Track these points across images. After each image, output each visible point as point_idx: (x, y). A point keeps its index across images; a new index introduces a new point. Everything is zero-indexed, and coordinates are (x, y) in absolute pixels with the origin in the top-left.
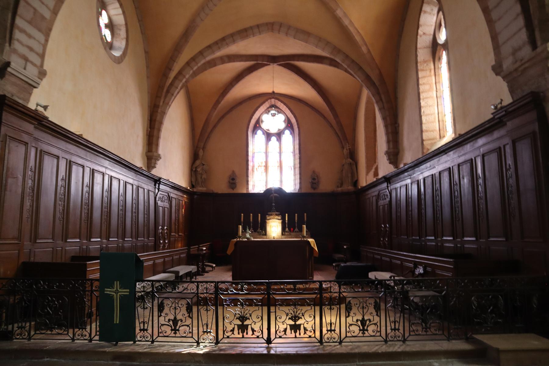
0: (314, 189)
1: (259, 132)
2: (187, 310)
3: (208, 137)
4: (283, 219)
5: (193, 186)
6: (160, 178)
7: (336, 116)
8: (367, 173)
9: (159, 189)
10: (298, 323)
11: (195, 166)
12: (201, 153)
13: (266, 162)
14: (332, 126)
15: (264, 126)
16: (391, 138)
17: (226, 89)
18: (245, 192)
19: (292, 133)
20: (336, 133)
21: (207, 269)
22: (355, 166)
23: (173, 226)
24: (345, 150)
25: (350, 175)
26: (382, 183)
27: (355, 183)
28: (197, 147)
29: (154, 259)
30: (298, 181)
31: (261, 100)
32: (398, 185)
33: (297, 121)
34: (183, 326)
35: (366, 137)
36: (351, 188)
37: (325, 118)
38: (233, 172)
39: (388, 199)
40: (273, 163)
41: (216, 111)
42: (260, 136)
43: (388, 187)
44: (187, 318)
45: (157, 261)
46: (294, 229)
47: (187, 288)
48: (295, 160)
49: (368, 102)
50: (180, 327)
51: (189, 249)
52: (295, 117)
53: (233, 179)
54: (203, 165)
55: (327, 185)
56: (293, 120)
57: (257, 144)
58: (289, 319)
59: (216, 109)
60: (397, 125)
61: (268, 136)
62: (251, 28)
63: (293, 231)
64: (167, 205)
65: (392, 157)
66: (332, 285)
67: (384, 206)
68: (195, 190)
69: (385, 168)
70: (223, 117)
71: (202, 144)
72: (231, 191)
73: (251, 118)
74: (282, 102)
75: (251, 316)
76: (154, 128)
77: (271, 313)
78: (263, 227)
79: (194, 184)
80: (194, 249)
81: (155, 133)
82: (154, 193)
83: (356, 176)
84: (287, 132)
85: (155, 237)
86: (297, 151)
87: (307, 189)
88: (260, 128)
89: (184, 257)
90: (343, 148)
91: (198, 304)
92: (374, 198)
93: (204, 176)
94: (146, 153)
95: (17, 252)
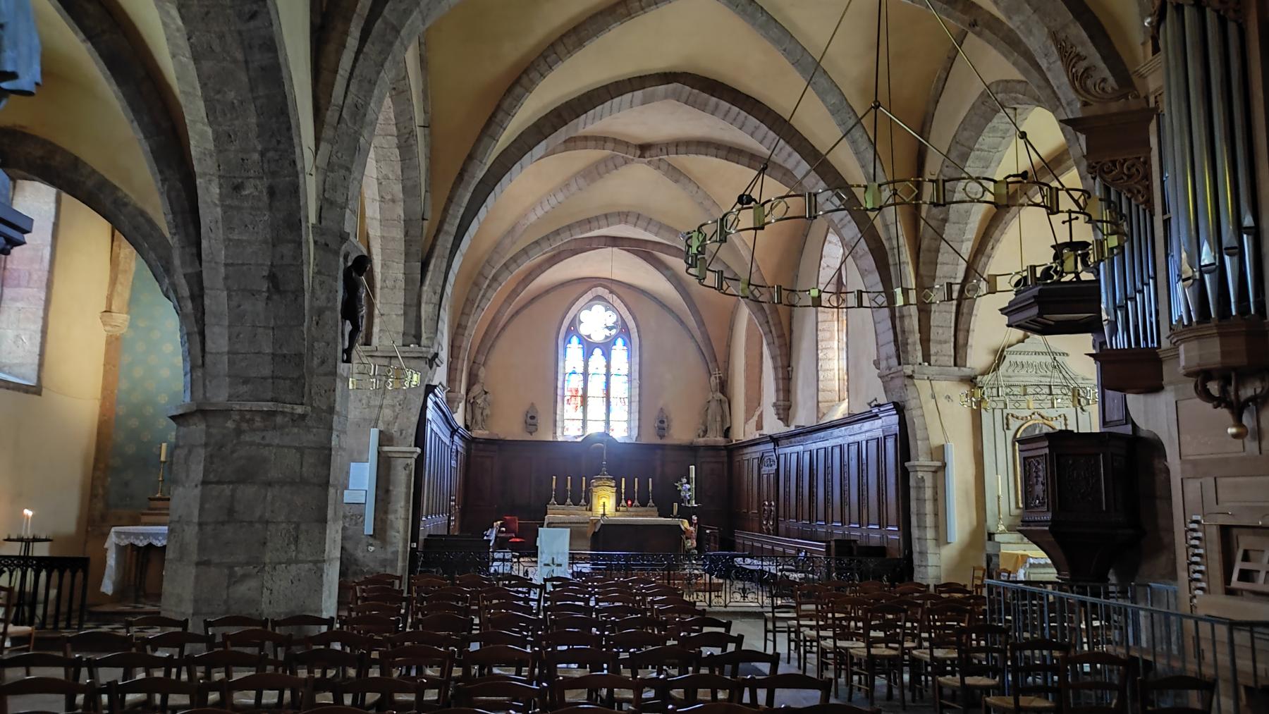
0: (662, 437)
1: (575, 340)
4: (618, 486)
7: (701, 323)
8: (747, 420)
11: (471, 395)
12: (482, 373)
13: (585, 389)
15: (583, 330)
17: (530, 274)
19: (628, 344)
25: (719, 419)
26: (767, 442)
27: (727, 433)
31: (580, 288)
32: (788, 450)
36: (720, 440)
37: (682, 322)
48: (630, 388)
49: (750, 320)
55: (681, 433)
57: (573, 356)
61: (588, 347)
62: (597, 218)
67: (768, 475)
69: (773, 426)
72: (528, 437)
78: (586, 500)
84: (620, 342)
86: (636, 375)
91: (728, 543)
93: (487, 412)
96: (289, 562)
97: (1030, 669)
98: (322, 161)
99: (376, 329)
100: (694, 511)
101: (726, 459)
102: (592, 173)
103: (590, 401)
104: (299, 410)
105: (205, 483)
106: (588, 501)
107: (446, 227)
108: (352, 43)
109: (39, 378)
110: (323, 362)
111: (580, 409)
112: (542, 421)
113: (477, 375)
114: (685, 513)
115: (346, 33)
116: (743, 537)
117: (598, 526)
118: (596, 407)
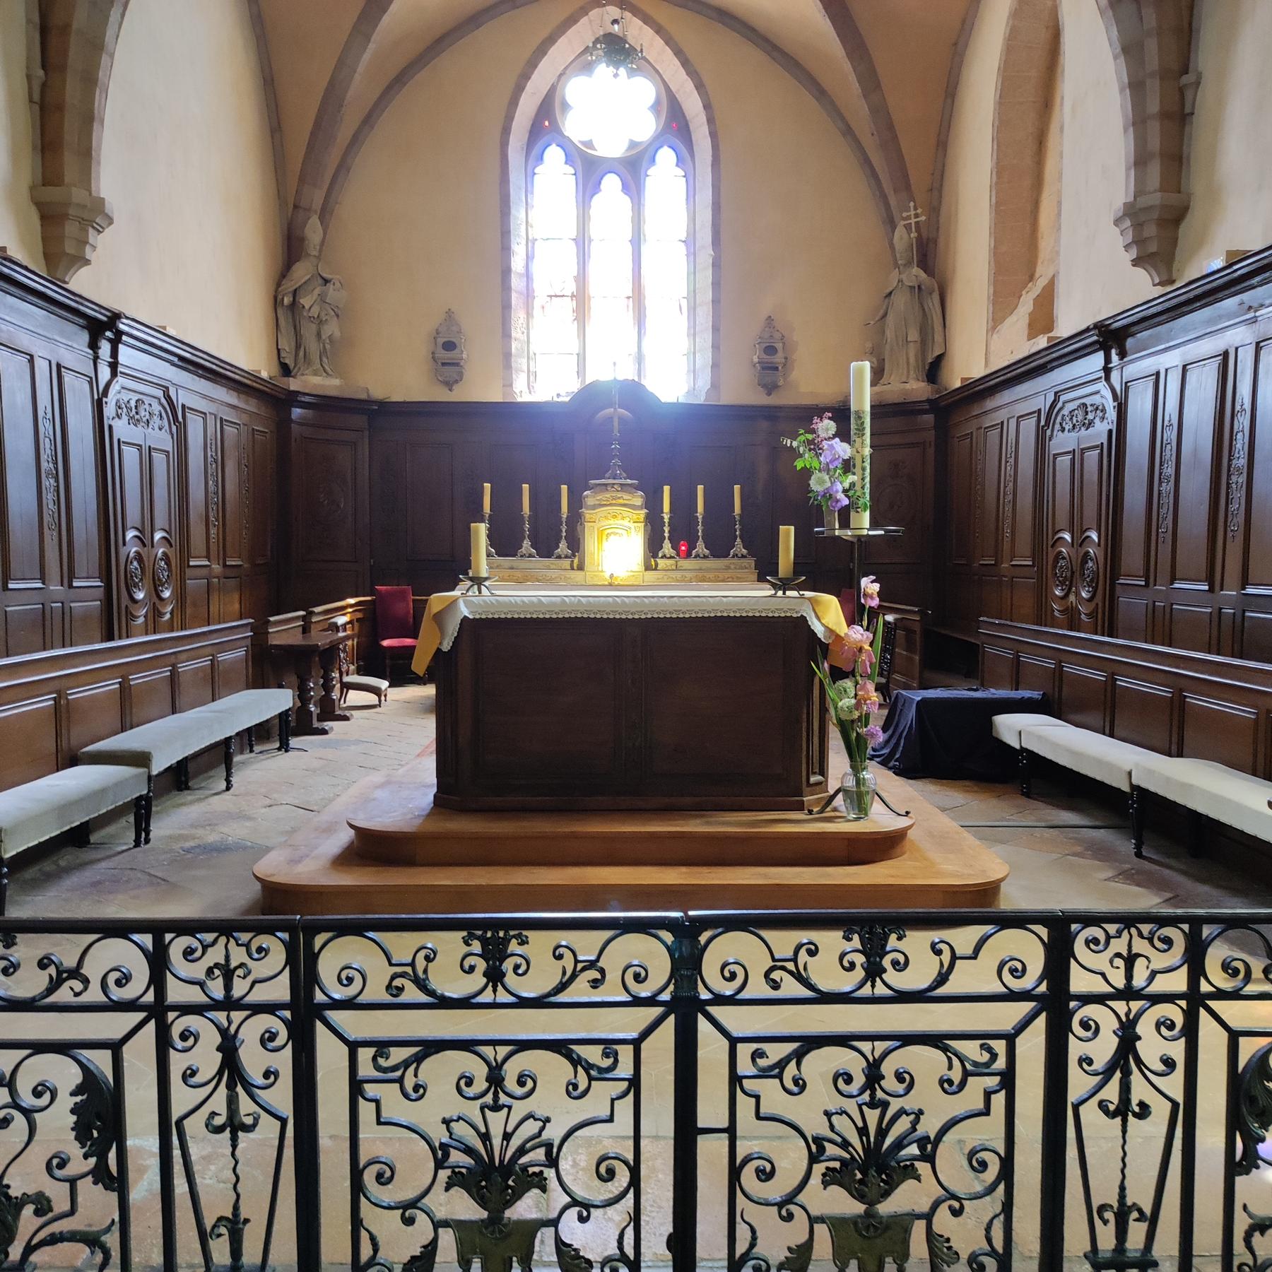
0: (771, 388)
1: (554, 154)
2: (81, 1132)
3: (343, 167)
5: (286, 370)
6: (116, 316)
7: (871, 82)
8: (996, 321)
9: (114, 366)
10: (886, 1208)
11: (289, 285)
12: (313, 232)
13: (581, 279)
14: (848, 131)
15: (574, 126)
16: (1155, 143)
18: (494, 395)
19: (686, 158)
20: (866, 162)
21: (354, 697)
22: (936, 297)
23: (197, 531)
24: (900, 232)
25: (914, 335)
27: (933, 371)
28: (296, 207)
29: (59, 689)
30: (705, 358)
32: (1172, 360)
33: (707, 107)
34: (53, 1240)
35: (1001, 170)
37: (820, 92)
38: (449, 313)
39: (1102, 429)
40: (605, 273)
41: (372, 46)
42: (554, 174)
43: (1107, 370)
44: (85, 1186)
45: (76, 694)
46: (692, 546)
47: (75, 973)
48: (693, 273)
50: (29, 1249)
51: (260, 631)
52: (700, 86)
53: (449, 346)
54: (326, 281)
56: (693, 105)
57: (546, 198)
58: (830, 1178)
59: (368, 39)
60: (1185, 79)
61: (589, 170)
63: (688, 555)
64: (161, 438)
65: (1151, 230)
66: (1140, 946)
67: (1077, 456)
68: (294, 385)
70: (400, 80)
71: (317, 198)
73: (519, 89)
75: (553, 1162)
76: (63, 68)
77: (703, 1143)
78: (557, 536)
79: (289, 361)
80: (285, 630)
81: (72, 90)
82: (93, 381)
83: (938, 337)
84: (666, 156)
85: (106, 574)
86: (705, 236)
87: (742, 391)
88: (556, 130)
89: (235, 661)
90: (891, 223)
92: (1029, 426)
93: (332, 328)
94: (32, 188)
95: (75, 584)
100: (863, 556)
101: (930, 436)
103: (597, 307)
106: (576, 545)
112: (474, 356)
113: (302, 240)
114: (828, 567)
116: (998, 634)
117: (452, 628)
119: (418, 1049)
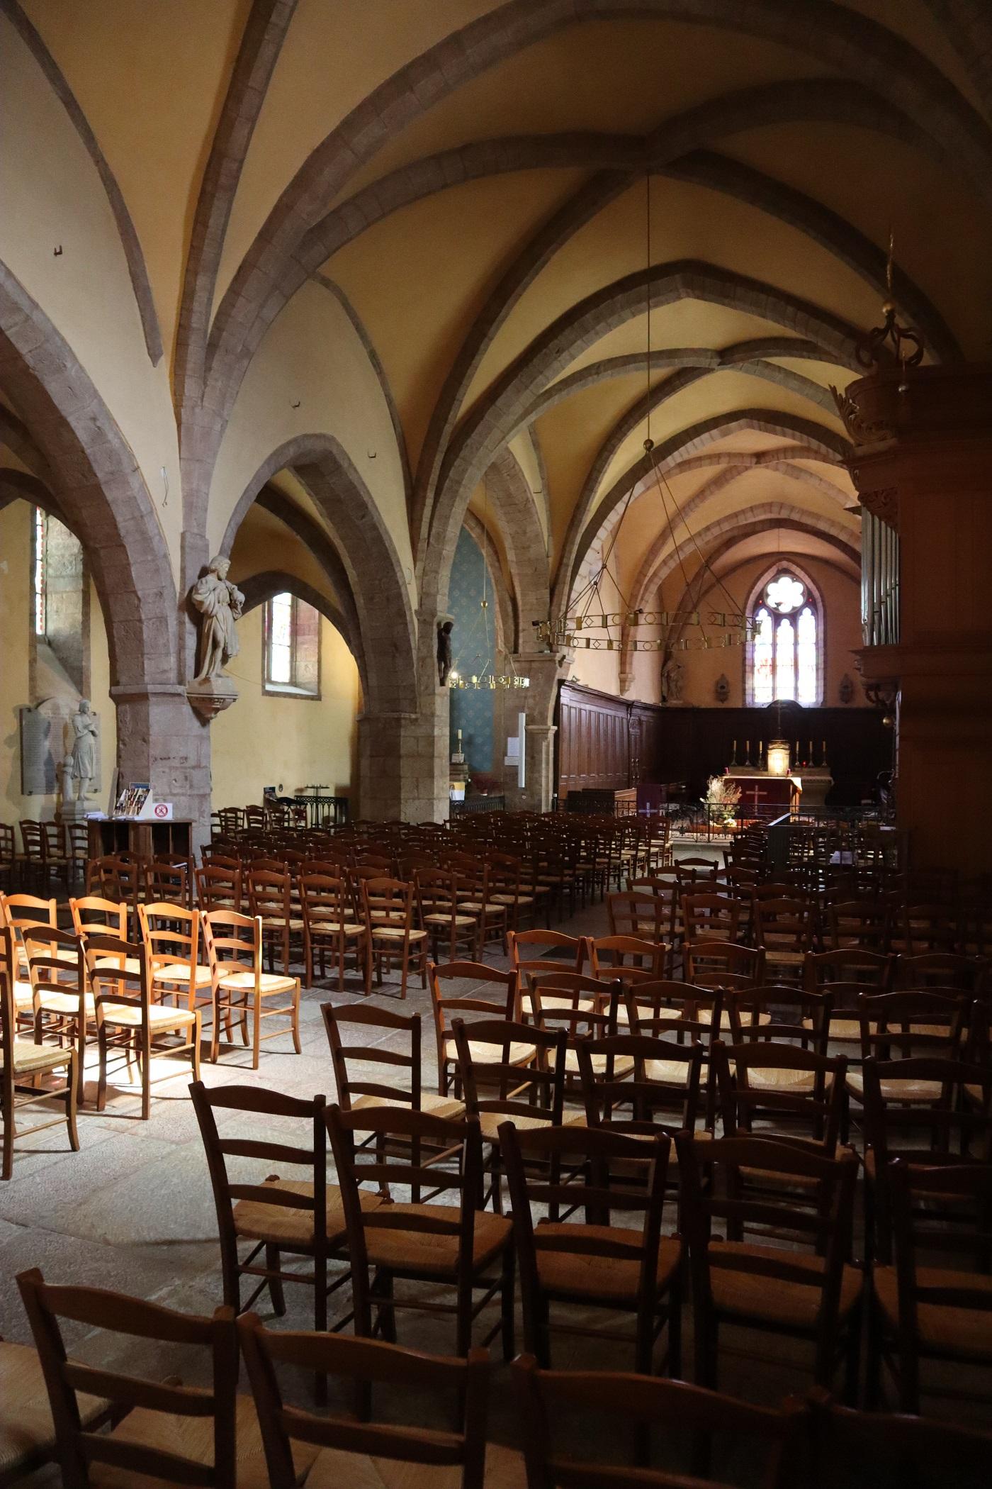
5: (664, 699)
15: (771, 602)
31: (765, 563)
52: (818, 588)
56: (816, 594)
61: (777, 617)
72: (846, 706)
74: (798, 565)
87: (836, 703)
96: (414, 799)
97: (754, 878)
98: (420, 572)
99: (521, 641)
102: (718, 482)
103: (779, 670)
104: (413, 716)
105: (372, 756)
107: (565, 561)
108: (429, 501)
109: (319, 690)
110: (427, 688)
111: (771, 677)
115: (425, 497)
118: (785, 671)
119: (769, 360)
